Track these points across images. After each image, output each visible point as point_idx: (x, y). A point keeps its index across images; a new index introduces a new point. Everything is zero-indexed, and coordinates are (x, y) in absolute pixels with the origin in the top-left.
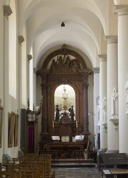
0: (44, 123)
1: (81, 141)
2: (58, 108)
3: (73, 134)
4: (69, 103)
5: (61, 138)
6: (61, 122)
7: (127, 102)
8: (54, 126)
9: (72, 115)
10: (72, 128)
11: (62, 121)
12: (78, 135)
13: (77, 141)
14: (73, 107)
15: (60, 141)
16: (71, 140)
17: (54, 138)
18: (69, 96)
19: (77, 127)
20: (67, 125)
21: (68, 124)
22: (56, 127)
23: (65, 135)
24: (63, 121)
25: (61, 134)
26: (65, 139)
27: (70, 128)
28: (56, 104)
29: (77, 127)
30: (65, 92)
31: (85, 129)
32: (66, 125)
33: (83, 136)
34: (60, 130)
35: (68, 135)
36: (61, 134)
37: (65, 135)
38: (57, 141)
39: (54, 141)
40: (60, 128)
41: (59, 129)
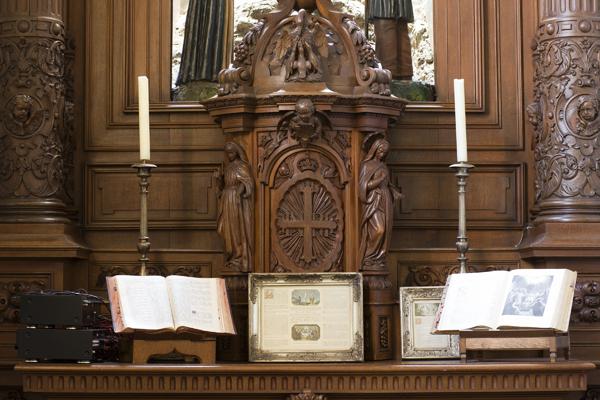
0: (24, 98)
1: (541, 354)
3: (410, 255)
5: (239, 309)
6: (248, 80)
7: (29, 387)
8: (140, 202)
10: (396, 170)
11: (261, 69)
12: (479, 264)
13: (471, 355)
15: (235, 345)
16: (381, 331)
17: (146, 302)
19: (462, 154)
20: (325, 119)
21: (351, 109)
22: (185, 168)
23: (304, 267)
25: (253, 249)
26: (305, 316)
27: (369, 173)
29: (462, 154)
31: (571, 185)
32: (320, 126)
34: (232, 196)
35: (338, 269)
36: (253, 249)
37: (305, 264)
38: (185, 347)
39: (140, 349)
40: (240, 173)
41: (222, 184)
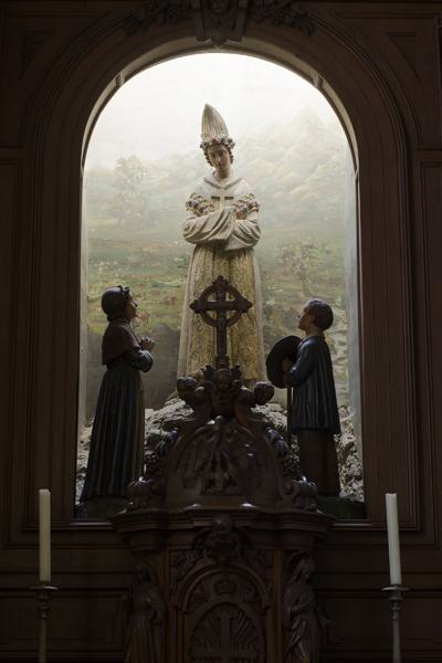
2: (127, 337)
4: (268, 311)
6: (158, 493)
9: (316, 417)
14: (320, 317)
18: (274, 234)
19: (395, 575)
24: (196, 491)
28: (94, 284)
29: (395, 575)
30: (223, 173)
33: (363, 500)
